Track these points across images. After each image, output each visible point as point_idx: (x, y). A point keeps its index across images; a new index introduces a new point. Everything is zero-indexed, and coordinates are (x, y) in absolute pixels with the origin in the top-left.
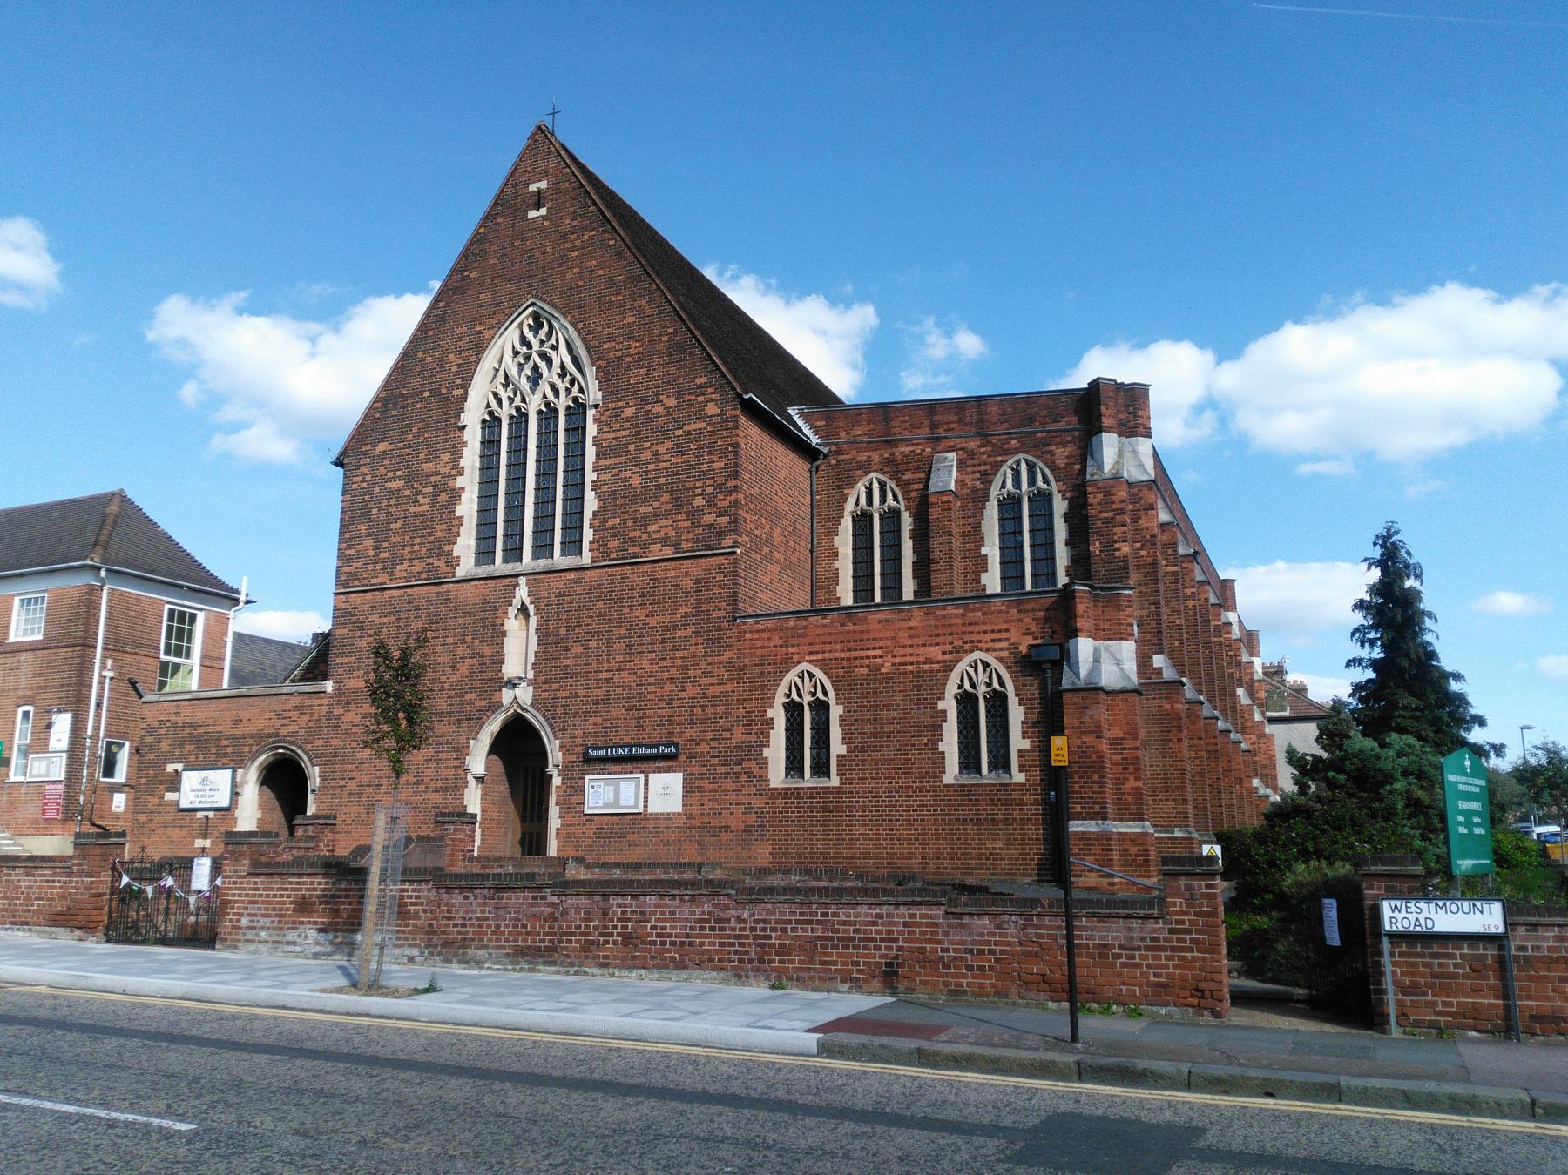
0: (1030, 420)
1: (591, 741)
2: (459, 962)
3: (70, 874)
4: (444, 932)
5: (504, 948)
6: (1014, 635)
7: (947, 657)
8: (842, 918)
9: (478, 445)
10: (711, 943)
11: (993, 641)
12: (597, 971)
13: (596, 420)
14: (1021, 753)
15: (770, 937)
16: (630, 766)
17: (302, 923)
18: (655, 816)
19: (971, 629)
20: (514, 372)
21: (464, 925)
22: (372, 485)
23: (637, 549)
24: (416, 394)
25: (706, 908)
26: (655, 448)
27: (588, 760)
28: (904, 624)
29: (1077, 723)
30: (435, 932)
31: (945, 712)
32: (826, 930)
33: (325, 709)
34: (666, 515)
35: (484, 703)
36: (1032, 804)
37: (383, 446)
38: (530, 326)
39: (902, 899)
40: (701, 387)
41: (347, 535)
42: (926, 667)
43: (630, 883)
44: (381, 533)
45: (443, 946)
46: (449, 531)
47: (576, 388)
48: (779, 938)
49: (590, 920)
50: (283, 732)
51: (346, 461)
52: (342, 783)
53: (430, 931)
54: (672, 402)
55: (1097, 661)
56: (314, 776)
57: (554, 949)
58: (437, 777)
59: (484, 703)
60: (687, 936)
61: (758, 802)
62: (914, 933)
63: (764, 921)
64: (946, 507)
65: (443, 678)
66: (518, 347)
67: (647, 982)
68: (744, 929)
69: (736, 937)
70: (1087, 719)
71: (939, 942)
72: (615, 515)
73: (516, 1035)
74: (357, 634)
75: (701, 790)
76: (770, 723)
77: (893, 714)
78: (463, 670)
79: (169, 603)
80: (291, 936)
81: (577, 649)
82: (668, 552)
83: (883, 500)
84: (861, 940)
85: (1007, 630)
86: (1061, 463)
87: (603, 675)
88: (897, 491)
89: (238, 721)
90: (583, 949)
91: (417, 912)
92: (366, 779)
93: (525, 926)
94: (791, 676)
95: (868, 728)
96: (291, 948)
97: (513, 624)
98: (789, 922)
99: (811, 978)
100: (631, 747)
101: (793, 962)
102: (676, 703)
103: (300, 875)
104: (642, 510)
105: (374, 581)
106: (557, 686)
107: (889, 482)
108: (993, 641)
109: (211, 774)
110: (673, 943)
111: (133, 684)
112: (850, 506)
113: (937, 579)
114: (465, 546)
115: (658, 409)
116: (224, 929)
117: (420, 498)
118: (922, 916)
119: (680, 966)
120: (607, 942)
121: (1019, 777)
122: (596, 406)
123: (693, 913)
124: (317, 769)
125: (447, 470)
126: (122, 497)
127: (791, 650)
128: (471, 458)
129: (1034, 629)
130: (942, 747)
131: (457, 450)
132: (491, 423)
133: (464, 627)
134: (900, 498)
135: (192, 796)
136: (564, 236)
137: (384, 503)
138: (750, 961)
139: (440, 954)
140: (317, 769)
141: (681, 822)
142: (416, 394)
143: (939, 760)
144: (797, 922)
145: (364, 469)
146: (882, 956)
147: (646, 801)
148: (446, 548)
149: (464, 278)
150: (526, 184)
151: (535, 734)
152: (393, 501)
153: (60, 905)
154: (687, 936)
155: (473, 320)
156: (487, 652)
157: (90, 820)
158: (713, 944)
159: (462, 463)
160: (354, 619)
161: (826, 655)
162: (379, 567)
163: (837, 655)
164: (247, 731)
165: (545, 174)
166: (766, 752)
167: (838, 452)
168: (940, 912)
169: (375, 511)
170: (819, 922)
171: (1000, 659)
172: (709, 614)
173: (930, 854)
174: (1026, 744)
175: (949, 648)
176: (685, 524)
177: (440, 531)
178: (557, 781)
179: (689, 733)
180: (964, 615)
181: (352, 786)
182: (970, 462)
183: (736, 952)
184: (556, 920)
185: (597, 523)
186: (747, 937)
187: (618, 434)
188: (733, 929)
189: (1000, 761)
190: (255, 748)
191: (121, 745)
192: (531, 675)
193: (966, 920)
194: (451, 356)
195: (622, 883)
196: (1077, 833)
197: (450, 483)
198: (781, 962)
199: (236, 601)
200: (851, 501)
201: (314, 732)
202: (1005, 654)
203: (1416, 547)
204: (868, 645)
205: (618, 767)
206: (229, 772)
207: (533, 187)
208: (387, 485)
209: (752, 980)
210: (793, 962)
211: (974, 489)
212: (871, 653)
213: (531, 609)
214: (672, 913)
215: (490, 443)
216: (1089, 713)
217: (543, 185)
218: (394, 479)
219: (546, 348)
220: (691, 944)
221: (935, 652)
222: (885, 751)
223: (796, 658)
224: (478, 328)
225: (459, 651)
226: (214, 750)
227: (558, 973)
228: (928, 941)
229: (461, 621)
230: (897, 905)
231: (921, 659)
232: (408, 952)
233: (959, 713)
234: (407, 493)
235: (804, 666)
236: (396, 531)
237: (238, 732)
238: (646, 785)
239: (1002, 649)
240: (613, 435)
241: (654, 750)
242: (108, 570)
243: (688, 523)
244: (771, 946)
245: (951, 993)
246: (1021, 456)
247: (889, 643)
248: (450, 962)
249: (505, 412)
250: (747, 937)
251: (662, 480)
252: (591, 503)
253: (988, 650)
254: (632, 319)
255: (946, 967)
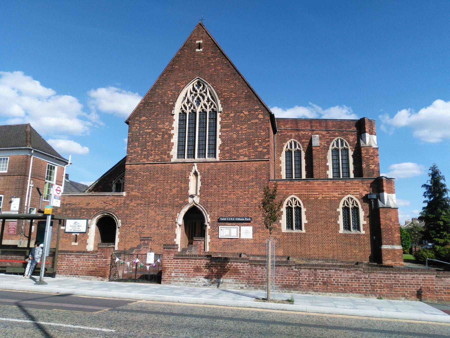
0: (342, 127)
1: (220, 216)
2: (261, 289)
3: (97, 257)
4: (255, 279)
5: (278, 285)
6: (361, 190)
7: (340, 196)
8: (401, 278)
9: (178, 121)
10: (355, 285)
11: (354, 192)
12: (314, 293)
13: (220, 116)
14: (364, 225)
15: (376, 283)
16: (234, 224)
17: (197, 275)
18: (243, 240)
19: (347, 188)
20: (191, 99)
21: (262, 277)
22: (140, 130)
23: (235, 157)
24: (156, 103)
25: (353, 274)
26: (241, 126)
27: (219, 221)
28: (326, 185)
29: (384, 217)
30: (251, 279)
31: (339, 212)
32: (396, 281)
33: (123, 201)
34: (245, 147)
35: (182, 202)
36: (368, 240)
37: (143, 118)
38: (196, 85)
39: (421, 273)
40: (257, 109)
41: (130, 146)
42: (333, 198)
43: (325, 266)
44: (144, 146)
45: (254, 284)
46: (169, 147)
47: (213, 106)
48: (380, 284)
49: (310, 277)
50: (107, 208)
51: (130, 122)
52: (130, 225)
53: (249, 279)
54: (247, 113)
55: (388, 199)
56: (119, 223)
57: (298, 286)
58: (165, 224)
59: (182, 202)
60: (347, 282)
61: (278, 236)
62: (426, 282)
63: (374, 279)
64: (318, 151)
65: (167, 193)
66: (192, 91)
67: (321, 296)
68: (367, 281)
69: (364, 283)
70: (387, 216)
71: (434, 285)
72: (227, 146)
73: (189, 305)
74: (135, 177)
75: (259, 232)
76: (282, 213)
77: (323, 212)
78: (174, 191)
79: (49, 162)
80: (193, 279)
81: (215, 187)
82: (246, 159)
83: (295, 147)
84: (408, 284)
85: (358, 189)
86: (351, 141)
87: (225, 195)
88: (300, 145)
89: (88, 204)
90: (308, 286)
91: (243, 272)
92: (139, 224)
93: (286, 278)
94: (289, 199)
95: (315, 216)
96: (193, 284)
97: (192, 178)
98: (383, 279)
99: (391, 296)
100: (235, 218)
101: (385, 291)
102: (250, 205)
103: (195, 259)
104: (237, 145)
105: (141, 161)
106: (208, 198)
107: (297, 142)
108: (354, 192)
109: (78, 221)
110: (341, 285)
111: (38, 189)
112: (285, 148)
113: (315, 172)
114: (174, 152)
115: (242, 115)
116: (164, 277)
117: (158, 136)
118: (428, 277)
119: (344, 292)
120: (317, 284)
121: (363, 232)
122: (221, 112)
123: (348, 276)
124: (120, 221)
125: (168, 128)
126: (28, 125)
127: (288, 191)
128: (176, 124)
129: (367, 189)
130: (338, 222)
131: (171, 122)
132: (183, 114)
133: (174, 177)
134: (301, 147)
135: (70, 228)
136: (209, 58)
137: (144, 136)
138: (369, 291)
139: (253, 286)
140: (120, 221)
141: (252, 241)
142: (156, 103)
143: (338, 226)
144: (386, 279)
145: (136, 125)
146: (415, 289)
147: (240, 235)
148: (168, 152)
149: (173, 68)
150: (195, 41)
151: (200, 213)
152: (148, 136)
153: (92, 268)
154: (347, 282)
155: (176, 81)
156: (183, 186)
157: (24, 235)
158: (356, 285)
159: (173, 126)
160: (134, 173)
161: (300, 193)
162: (143, 156)
163: (304, 193)
164: (92, 207)
165: (202, 38)
166: (280, 221)
167: (281, 132)
168: (434, 276)
169: (141, 139)
170: (393, 279)
171: (357, 197)
172: (260, 179)
173: (335, 253)
174: (365, 223)
175: (341, 193)
176: (252, 151)
177: (165, 147)
178: (209, 227)
179: (254, 214)
180: (345, 184)
181: (134, 226)
182: (323, 138)
183: (364, 288)
184: (297, 276)
185: (221, 148)
186: (368, 283)
187: (228, 121)
188: (363, 281)
189: (357, 227)
190: (95, 213)
191: (33, 209)
192: (199, 194)
193: (443, 279)
194: (169, 92)
195: (259, 261)
196: (385, 249)
197: (169, 132)
198: (380, 291)
199: (67, 163)
200: (285, 147)
201: (118, 209)
202: (358, 196)
203: (443, 172)
204: (314, 191)
205: (230, 224)
206: (86, 221)
207: (197, 42)
208: (145, 131)
209: (370, 296)
210: (385, 291)
211: (324, 146)
212: (315, 193)
213: (199, 173)
214: (341, 275)
215: (182, 120)
216: (388, 214)
217: (201, 42)
218: (148, 129)
219: (202, 92)
220: (348, 285)
221: (336, 194)
222: (320, 223)
223: (290, 193)
224: (178, 84)
225: (173, 185)
226: (79, 213)
227: (299, 293)
228: (430, 285)
229: (173, 176)
230: (420, 274)
231: (331, 196)
232: (241, 285)
233: (343, 212)
234: (153, 134)
235: (293, 196)
236: (149, 146)
237: (89, 207)
238: (240, 230)
239: (357, 194)
240: (227, 121)
241: (243, 219)
242: (34, 151)
243: (253, 150)
244: (377, 286)
245: (439, 300)
246: (339, 137)
247: (321, 191)
248: (257, 289)
249: (188, 111)
250: (368, 283)
251: (244, 137)
252: (219, 142)
253: (353, 195)
254: (233, 87)
255: (436, 292)
